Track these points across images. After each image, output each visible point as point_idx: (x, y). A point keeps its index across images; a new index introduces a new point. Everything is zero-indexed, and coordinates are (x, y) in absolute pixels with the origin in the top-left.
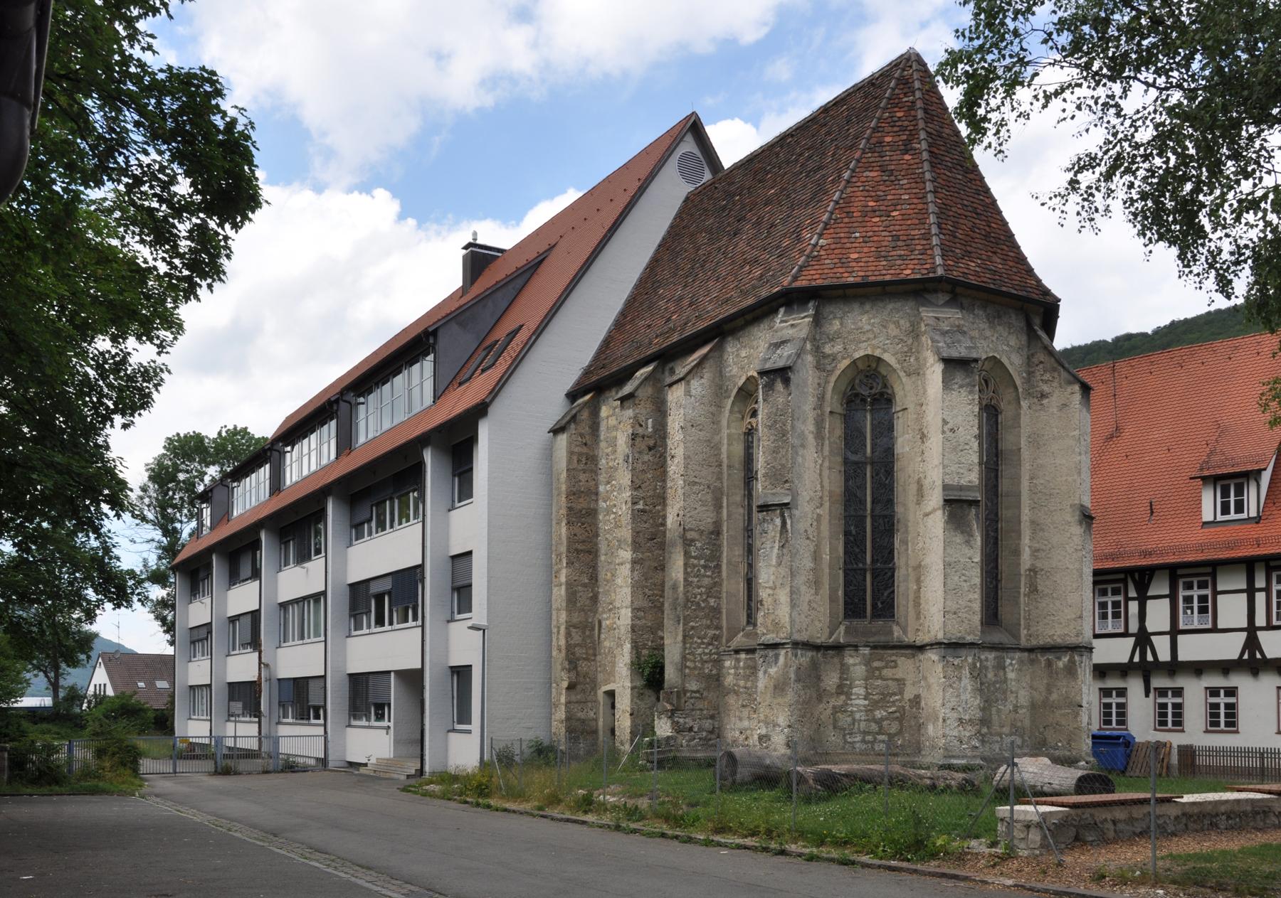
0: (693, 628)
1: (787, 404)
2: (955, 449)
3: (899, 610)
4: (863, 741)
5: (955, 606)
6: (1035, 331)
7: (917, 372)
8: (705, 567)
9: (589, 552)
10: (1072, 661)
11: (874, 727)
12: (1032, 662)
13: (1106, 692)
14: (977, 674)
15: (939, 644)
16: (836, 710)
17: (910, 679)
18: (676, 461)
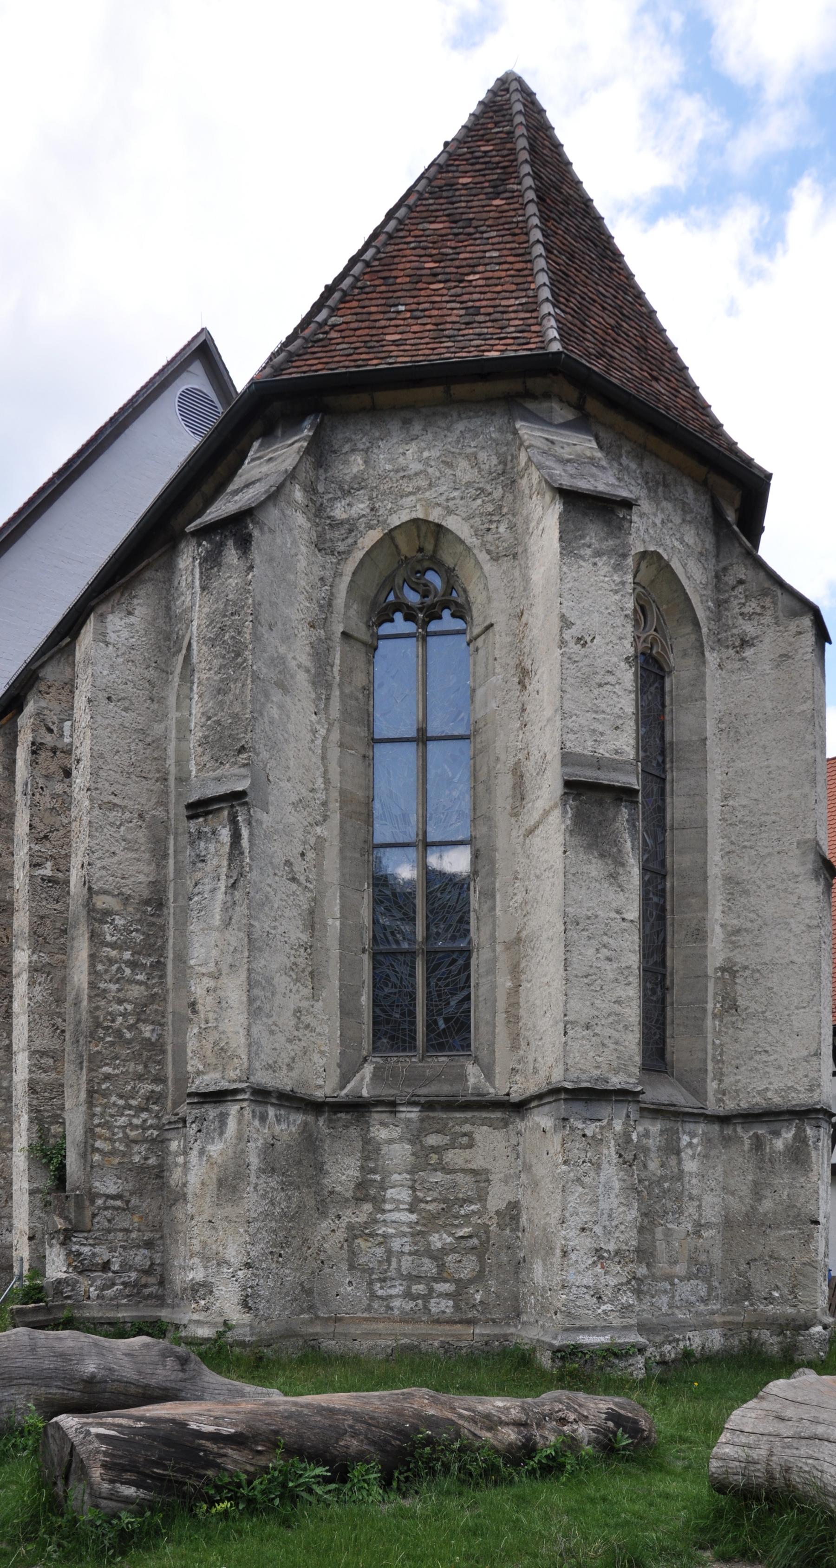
0: (107, 1077)
1: (245, 589)
2: (585, 680)
3: (478, 1034)
7: (513, 553)
11: (429, 1267)
12: (727, 1141)
14: (631, 1156)
15: (555, 1092)
16: (354, 1233)
17: (499, 1169)
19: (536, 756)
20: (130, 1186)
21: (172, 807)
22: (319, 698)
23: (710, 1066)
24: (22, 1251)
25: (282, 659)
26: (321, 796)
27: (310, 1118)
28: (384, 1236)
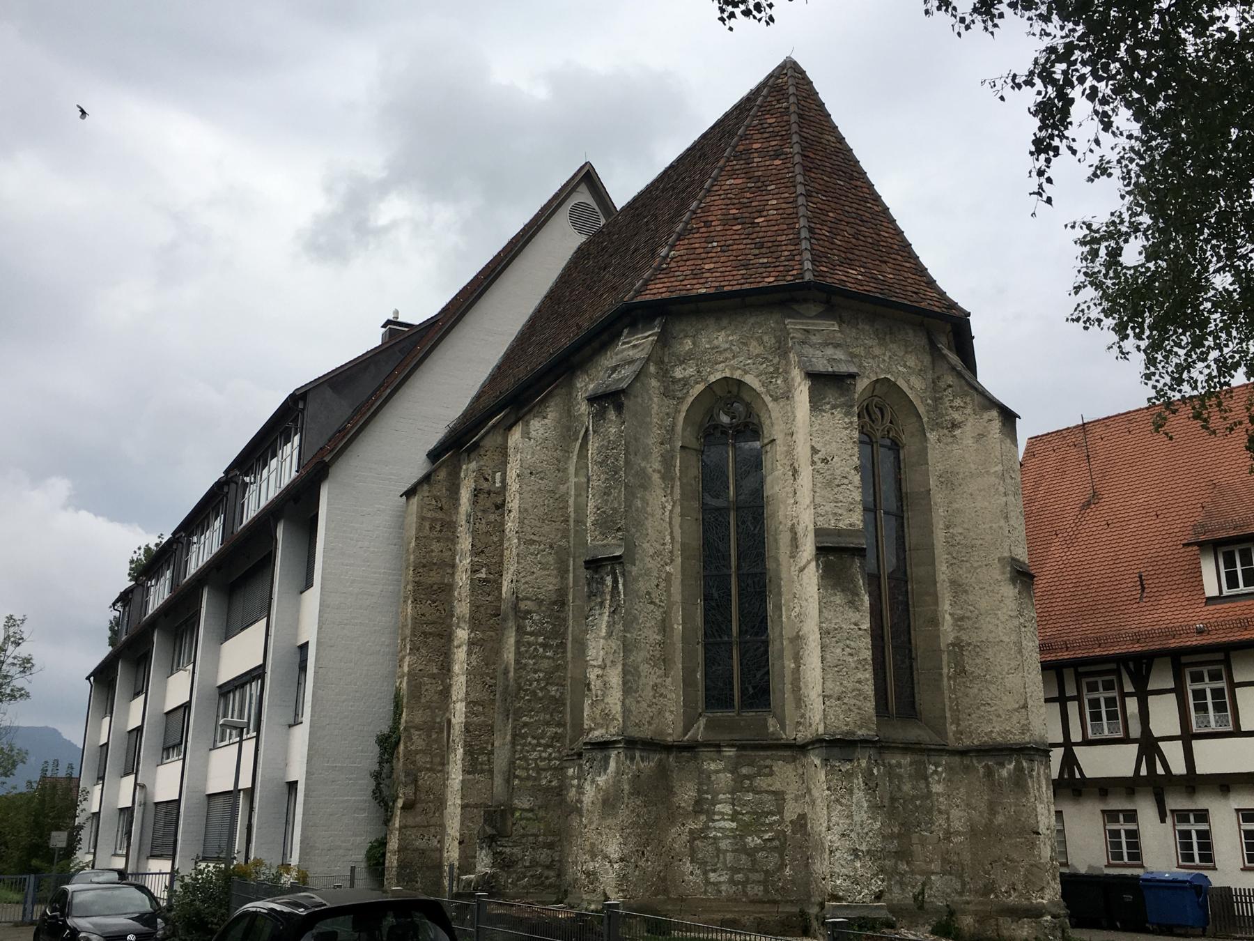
0: (525, 724)
2: (829, 484)
4: (732, 881)
5: (838, 689)
6: (939, 350)
7: (787, 396)
8: (545, 646)
9: (441, 636)
10: (1019, 769)
12: (967, 769)
13: (1110, 816)
17: (792, 791)
18: (512, 515)
19: (802, 525)
20: (539, 802)
21: (571, 539)
22: (666, 486)
23: (948, 715)
24: (452, 853)
25: (644, 470)
26: (669, 547)
27: (664, 756)
28: (715, 838)
